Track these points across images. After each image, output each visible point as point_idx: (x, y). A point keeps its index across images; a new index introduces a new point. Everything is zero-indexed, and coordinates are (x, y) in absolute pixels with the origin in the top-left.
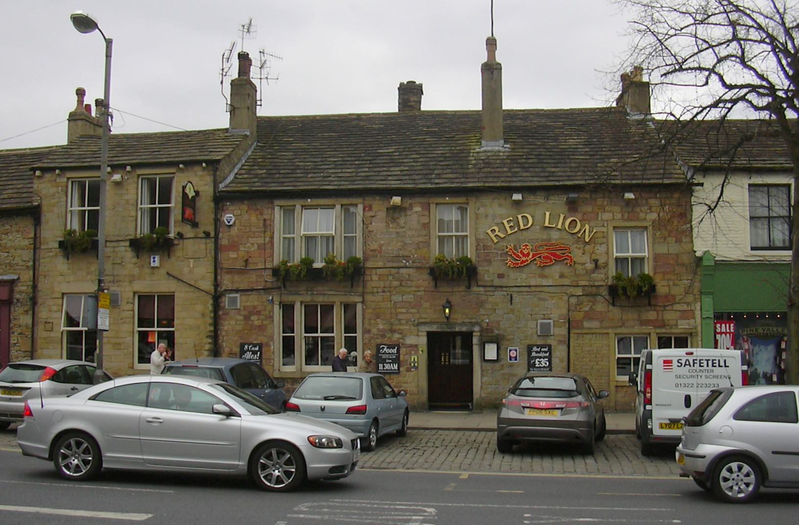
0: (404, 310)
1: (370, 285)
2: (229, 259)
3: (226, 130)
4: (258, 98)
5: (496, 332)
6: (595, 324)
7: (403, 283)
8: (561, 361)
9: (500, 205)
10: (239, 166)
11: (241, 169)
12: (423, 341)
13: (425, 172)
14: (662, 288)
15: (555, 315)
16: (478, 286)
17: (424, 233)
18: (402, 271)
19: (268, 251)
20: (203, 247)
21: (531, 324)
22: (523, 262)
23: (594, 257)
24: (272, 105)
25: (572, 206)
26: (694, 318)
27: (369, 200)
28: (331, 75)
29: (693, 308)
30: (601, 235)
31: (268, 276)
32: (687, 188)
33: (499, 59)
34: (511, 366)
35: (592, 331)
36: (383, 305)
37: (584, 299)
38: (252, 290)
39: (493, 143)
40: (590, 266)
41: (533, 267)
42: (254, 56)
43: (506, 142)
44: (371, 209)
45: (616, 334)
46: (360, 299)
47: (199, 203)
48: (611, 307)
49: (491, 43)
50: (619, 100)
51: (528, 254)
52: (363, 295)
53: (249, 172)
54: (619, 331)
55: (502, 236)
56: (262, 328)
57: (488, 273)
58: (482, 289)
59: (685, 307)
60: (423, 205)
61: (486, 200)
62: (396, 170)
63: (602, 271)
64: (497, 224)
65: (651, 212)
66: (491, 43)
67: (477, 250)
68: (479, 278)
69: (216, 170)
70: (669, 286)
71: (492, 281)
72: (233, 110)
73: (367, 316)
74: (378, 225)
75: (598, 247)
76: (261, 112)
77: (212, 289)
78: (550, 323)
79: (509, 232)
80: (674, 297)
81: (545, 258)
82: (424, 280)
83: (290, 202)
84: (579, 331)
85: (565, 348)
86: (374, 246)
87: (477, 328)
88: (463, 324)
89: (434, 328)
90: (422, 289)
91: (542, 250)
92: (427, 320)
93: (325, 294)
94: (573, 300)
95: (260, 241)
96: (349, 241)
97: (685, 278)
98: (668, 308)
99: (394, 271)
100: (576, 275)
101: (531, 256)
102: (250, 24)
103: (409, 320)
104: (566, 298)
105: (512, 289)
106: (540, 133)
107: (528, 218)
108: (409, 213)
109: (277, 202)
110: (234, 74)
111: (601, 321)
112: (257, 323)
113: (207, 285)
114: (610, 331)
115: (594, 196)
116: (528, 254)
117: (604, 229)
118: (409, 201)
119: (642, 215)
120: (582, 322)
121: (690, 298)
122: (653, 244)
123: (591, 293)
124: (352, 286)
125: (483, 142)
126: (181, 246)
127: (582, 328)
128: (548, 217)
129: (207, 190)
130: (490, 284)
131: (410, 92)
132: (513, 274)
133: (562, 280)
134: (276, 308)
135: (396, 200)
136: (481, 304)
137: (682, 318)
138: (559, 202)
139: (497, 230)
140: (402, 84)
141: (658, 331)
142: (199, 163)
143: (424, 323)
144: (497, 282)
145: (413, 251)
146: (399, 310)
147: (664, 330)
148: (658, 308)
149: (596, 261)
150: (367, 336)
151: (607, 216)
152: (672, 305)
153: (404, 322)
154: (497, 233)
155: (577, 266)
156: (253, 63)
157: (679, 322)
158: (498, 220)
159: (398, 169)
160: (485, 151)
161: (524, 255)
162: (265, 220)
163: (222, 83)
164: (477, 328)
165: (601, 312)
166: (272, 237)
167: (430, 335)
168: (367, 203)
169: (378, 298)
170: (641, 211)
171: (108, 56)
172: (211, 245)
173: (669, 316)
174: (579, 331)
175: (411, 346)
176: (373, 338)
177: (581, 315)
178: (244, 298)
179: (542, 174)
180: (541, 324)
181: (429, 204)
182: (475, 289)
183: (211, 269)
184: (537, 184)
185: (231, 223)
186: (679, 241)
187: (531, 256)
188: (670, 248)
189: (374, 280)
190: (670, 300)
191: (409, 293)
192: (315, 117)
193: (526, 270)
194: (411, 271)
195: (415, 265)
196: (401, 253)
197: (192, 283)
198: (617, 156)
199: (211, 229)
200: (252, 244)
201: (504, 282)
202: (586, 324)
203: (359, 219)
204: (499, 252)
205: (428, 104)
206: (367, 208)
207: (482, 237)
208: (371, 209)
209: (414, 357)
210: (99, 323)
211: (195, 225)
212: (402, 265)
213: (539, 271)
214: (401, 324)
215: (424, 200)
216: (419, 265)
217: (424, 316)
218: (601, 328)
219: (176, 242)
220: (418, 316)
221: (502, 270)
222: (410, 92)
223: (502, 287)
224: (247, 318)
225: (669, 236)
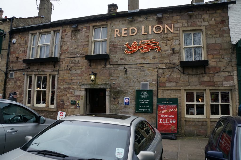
0: (75, 78)
1: (62, 66)
2: (13, 57)
4: (53, 7)
5: (118, 89)
6: (173, 84)
7: (76, 65)
9: (123, 24)
14: (212, 63)
15: (150, 79)
16: (110, 65)
17: (87, 40)
18: (76, 59)
22: (133, 51)
23: (172, 47)
26: (233, 80)
27: (65, 28)
29: (232, 74)
30: (176, 35)
34: (126, 107)
35: (171, 88)
36: (66, 75)
37: (166, 70)
40: (170, 52)
41: (138, 54)
44: (65, 31)
45: (185, 90)
48: (182, 75)
51: (136, 47)
54: (187, 88)
55: (119, 36)
56: (20, 86)
57: (115, 58)
58: (112, 66)
59: (227, 74)
63: (177, 54)
65: (204, 21)
67: (110, 46)
68: (110, 61)
70: (216, 62)
71: (117, 62)
73: (60, 81)
74: (67, 39)
75: (174, 41)
78: (147, 84)
80: (220, 68)
81: (145, 48)
82: (84, 62)
84: (163, 88)
86: (65, 48)
87: (108, 87)
89: (88, 87)
90: (84, 67)
92: (85, 83)
93: (43, 71)
94: (160, 71)
95: (23, 49)
97: (226, 57)
98: (216, 75)
99: (72, 59)
100: (163, 57)
101: (137, 48)
103: (77, 83)
104: (156, 70)
105: (127, 66)
108: (81, 31)
112: (19, 84)
113: (4, 69)
114: (182, 88)
115: (172, 15)
116: (136, 47)
117: (178, 32)
119: (199, 23)
120: (165, 83)
121: (230, 69)
122: (206, 38)
123: (171, 67)
124: (54, 67)
127: (166, 87)
130: (116, 63)
132: (128, 58)
133: (154, 60)
134: (26, 77)
137: (225, 80)
139: (118, 32)
141: (211, 88)
143: (83, 84)
144: (120, 62)
146: (73, 78)
147: (214, 88)
148: (210, 75)
149: (173, 49)
150: (59, 90)
151: (179, 25)
152: (218, 72)
153: (75, 84)
154: (117, 33)
155: (163, 52)
165: (176, 78)
167: (86, 90)
168: (64, 29)
170: (198, 21)
174: (163, 88)
176: (61, 91)
177: (165, 79)
180: (143, 84)
181: (90, 26)
182: (108, 66)
185: (14, 43)
186: (221, 36)
187: (137, 48)
188: (218, 40)
189: (63, 64)
190: (217, 70)
191: (78, 69)
193: (135, 55)
194: (79, 59)
195: (82, 56)
196: (76, 50)
200: (21, 51)
201: (123, 62)
202: (168, 85)
204: (121, 47)
206: (64, 31)
207: (113, 40)
212: (76, 56)
213: (141, 56)
214: (74, 85)
217: (84, 80)
218: (177, 86)
220: (81, 81)
221: (122, 56)
223: (122, 65)
224: (16, 82)
225: (215, 34)
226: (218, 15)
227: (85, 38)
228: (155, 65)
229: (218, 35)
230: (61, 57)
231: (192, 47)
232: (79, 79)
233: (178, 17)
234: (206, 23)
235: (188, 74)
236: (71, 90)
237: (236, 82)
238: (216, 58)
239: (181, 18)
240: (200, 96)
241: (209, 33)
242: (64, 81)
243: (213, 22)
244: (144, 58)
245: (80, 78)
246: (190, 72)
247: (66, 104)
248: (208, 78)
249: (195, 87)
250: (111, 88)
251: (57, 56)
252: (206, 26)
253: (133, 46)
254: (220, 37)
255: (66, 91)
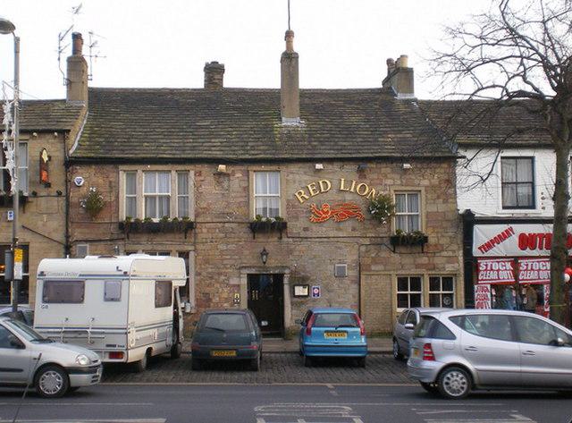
3: (64, 101)
6: (380, 267)
8: (354, 297)
9: (305, 173)
10: (80, 134)
11: (81, 136)
12: (244, 281)
13: (241, 144)
14: (432, 240)
15: (349, 261)
17: (244, 194)
18: (227, 225)
19: (113, 208)
20: (56, 204)
21: (331, 267)
24: (102, 76)
25: (361, 172)
28: (147, 56)
29: (456, 254)
31: (113, 228)
32: (452, 160)
33: (296, 48)
34: (314, 301)
37: (372, 247)
38: (100, 240)
39: (292, 120)
42: (85, 37)
43: (302, 119)
46: (192, 248)
47: (51, 167)
48: (393, 254)
49: (289, 35)
50: (385, 82)
52: (194, 244)
53: (90, 139)
54: (399, 272)
55: (307, 197)
57: (295, 227)
58: (291, 240)
59: (451, 254)
60: (242, 172)
61: (294, 168)
62: (217, 141)
64: (302, 188)
66: (289, 35)
69: (64, 139)
71: (299, 233)
72: (70, 83)
76: (91, 84)
77: (64, 241)
79: (313, 194)
80: (442, 245)
82: (244, 233)
83: (133, 168)
85: (356, 286)
88: (277, 267)
89: (253, 271)
91: (337, 209)
94: (363, 249)
96: (184, 201)
102: (80, 7)
106: (329, 107)
107: (326, 183)
109: (121, 167)
110: (69, 52)
111: (385, 266)
114: (392, 272)
116: (327, 212)
118: (231, 169)
120: (370, 266)
121: (455, 247)
125: (283, 119)
126: (34, 203)
127: (370, 270)
128: (342, 185)
129: (59, 156)
131: (214, 71)
132: (314, 228)
135: (222, 167)
136: (290, 252)
138: (351, 169)
140: (207, 65)
141: (430, 272)
142: (51, 132)
143: (245, 267)
145: (236, 209)
147: (434, 272)
148: (429, 255)
151: (389, 182)
152: (440, 252)
156: (84, 42)
157: (447, 266)
158: (304, 185)
159: (217, 140)
160: (285, 126)
161: (325, 213)
162: (110, 182)
163: (59, 59)
164: (287, 271)
166: (117, 197)
167: (250, 277)
169: (207, 246)
171: (17, 52)
172: (62, 201)
173: (438, 261)
175: (234, 286)
178: (94, 247)
179: (336, 147)
182: (285, 239)
183: (63, 222)
184: (334, 156)
185: (81, 184)
186: (445, 201)
188: (440, 207)
189: (203, 232)
190: (439, 248)
192: (133, 89)
194: (233, 225)
197: (46, 235)
198: (391, 130)
199: (62, 189)
201: (309, 234)
202: (373, 268)
203: (191, 183)
205: (230, 81)
208: (200, 175)
209: (237, 295)
210: (15, 274)
211: (48, 185)
213: (336, 225)
214: (227, 269)
215: (244, 168)
216: (240, 220)
219: (30, 200)
221: (307, 224)
222: (214, 71)
223: (306, 238)
226: (442, 171)
227: (240, 190)
228: (356, 240)
229: (441, 200)
230: (199, 220)
231: (405, 215)
232: (235, 259)
233: (389, 170)
234: (426, 182)
235: (400, 253)
236: (223, 278)
237: (462, 265)
238: (437, 232)
239: (393, 172)
240: (416, 283)
241: (429, 196)
242: (207, 262)
243: (435, 181)
244: (339, 229)
245: (237, 257)
246: (403, 250)
247: (214, 301)
248: (427, 258)
249: (411, 271)
250: (291, 273)
251: (192, 218)
252: (426, 187)
253: (322, 211)
254: (444, 203)
255: (211, 278)
